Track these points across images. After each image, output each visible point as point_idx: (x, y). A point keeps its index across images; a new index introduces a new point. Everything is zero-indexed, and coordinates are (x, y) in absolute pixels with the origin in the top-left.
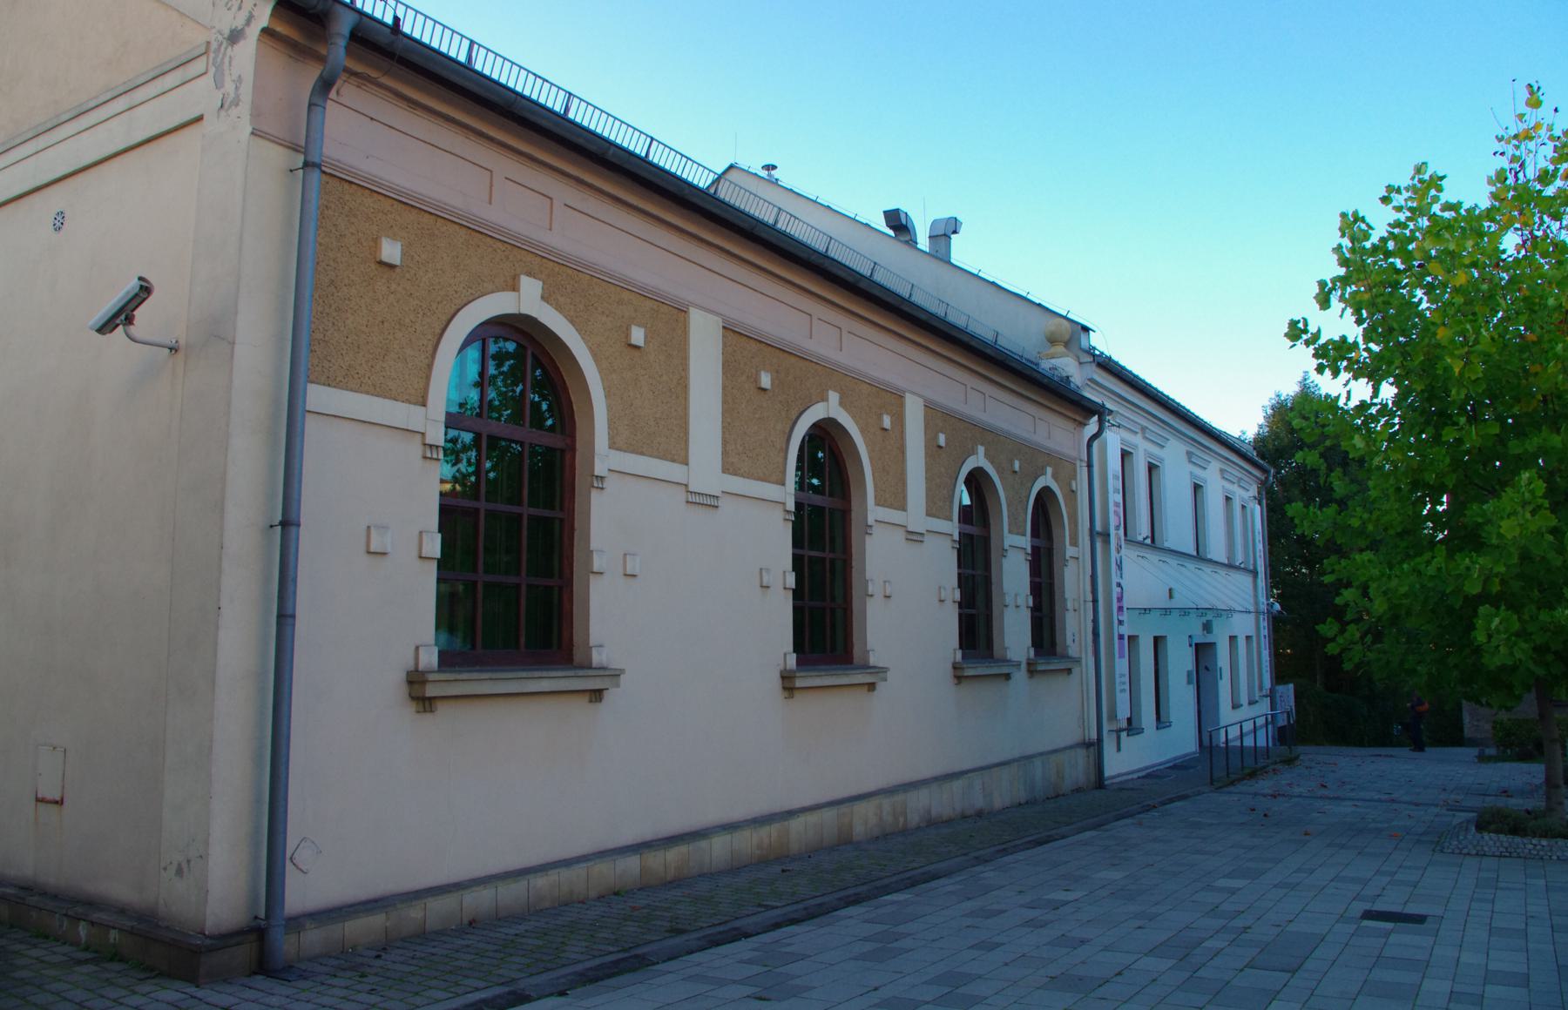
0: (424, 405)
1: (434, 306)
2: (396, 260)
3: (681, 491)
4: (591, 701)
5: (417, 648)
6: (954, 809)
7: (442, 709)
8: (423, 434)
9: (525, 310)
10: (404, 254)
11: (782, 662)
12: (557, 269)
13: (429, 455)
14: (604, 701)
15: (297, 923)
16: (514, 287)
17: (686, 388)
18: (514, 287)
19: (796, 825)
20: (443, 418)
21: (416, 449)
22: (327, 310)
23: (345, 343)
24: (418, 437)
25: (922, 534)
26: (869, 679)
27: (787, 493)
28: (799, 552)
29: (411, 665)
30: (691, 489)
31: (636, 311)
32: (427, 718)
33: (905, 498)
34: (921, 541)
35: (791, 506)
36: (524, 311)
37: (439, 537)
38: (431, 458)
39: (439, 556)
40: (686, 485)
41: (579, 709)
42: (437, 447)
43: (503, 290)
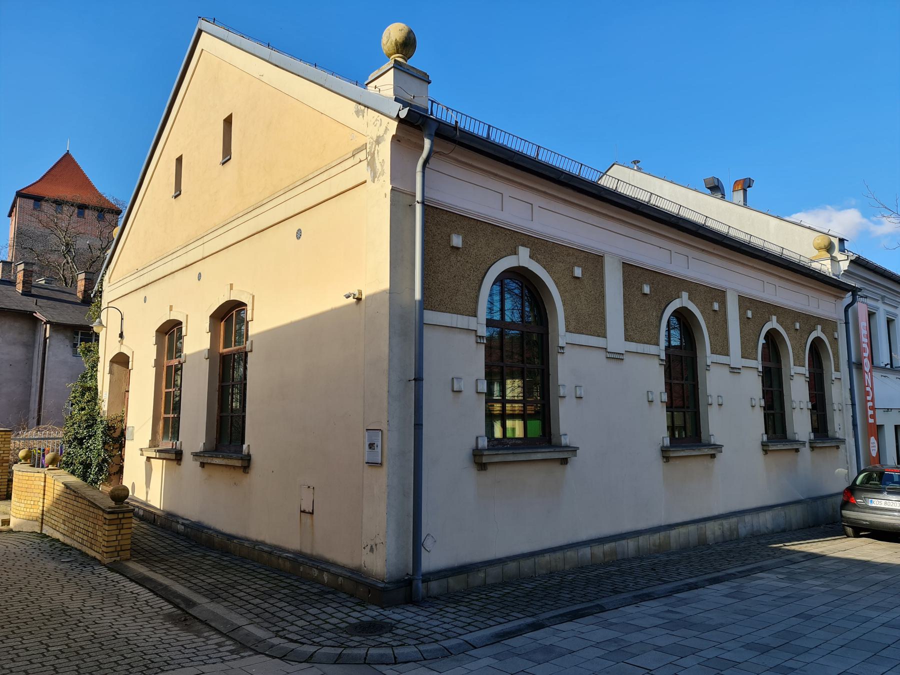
5: (477, 438)
8: (476, 331)
16: (515, 253)
21: (472, 338)
25: (739, 369)
33: (605, 330)
36: (521, 265)
42: (483, 337)
43: (511, 255)
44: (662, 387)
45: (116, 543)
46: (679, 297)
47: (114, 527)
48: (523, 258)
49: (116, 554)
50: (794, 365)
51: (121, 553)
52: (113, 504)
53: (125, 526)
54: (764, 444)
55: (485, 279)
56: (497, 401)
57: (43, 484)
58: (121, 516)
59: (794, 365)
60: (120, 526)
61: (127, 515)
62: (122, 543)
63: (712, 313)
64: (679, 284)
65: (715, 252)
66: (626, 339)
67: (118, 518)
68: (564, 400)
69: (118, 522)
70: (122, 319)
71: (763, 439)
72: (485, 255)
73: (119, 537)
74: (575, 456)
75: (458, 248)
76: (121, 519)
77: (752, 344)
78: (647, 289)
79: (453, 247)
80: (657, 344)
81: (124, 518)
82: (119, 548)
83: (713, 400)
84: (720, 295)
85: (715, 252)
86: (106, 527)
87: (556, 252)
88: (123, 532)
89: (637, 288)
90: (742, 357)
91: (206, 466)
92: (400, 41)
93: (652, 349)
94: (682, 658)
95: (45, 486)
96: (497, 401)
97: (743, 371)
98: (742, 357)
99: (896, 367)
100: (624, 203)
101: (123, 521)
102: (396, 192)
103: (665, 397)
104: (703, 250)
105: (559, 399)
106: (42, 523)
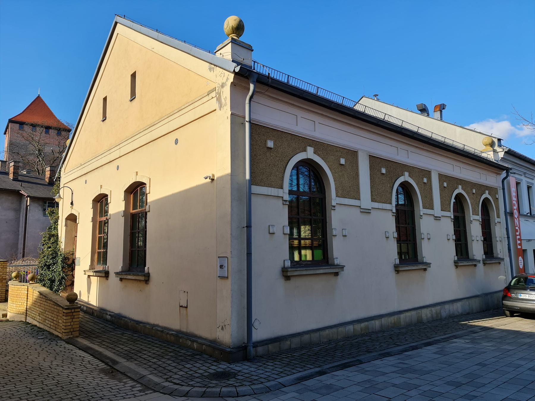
11: (394, 262)
13: (285, 203)
21: (281, 202)
24: (281, 198)
42: (287, 201)
44: (394, 229)
45: (70, 327)
47: (69, 317)
49: (70, 333)
50: (473, 215)
52: (68, 304)
53: (76, 317)
54: (455, 262)
56: (296, 239)
57: (26, 292)
58: (73, 311)
60: (72, 317)
61: (76, 310)
62: (74, 327)
63: (423, 184)
64: (403, 168)
66: (372, 201)
67: (71, 312)
69: (71, 314)
70: (72, 194)
71: (483, 258)
72: (287, 152)
73: (72, 324)
75: (271, 148)
79: (268, 148)
82: (72, 330)
83: (425, 236)
84: (353, 155)
86: (65, 318)
88: (74, 320)
90: (441, 210)
91: (123, 280)
95: (28, 294)
96: (296, 239)
97: (442, 219)
98: (441, 210)
101: (74, 314)
106: (26, 316)
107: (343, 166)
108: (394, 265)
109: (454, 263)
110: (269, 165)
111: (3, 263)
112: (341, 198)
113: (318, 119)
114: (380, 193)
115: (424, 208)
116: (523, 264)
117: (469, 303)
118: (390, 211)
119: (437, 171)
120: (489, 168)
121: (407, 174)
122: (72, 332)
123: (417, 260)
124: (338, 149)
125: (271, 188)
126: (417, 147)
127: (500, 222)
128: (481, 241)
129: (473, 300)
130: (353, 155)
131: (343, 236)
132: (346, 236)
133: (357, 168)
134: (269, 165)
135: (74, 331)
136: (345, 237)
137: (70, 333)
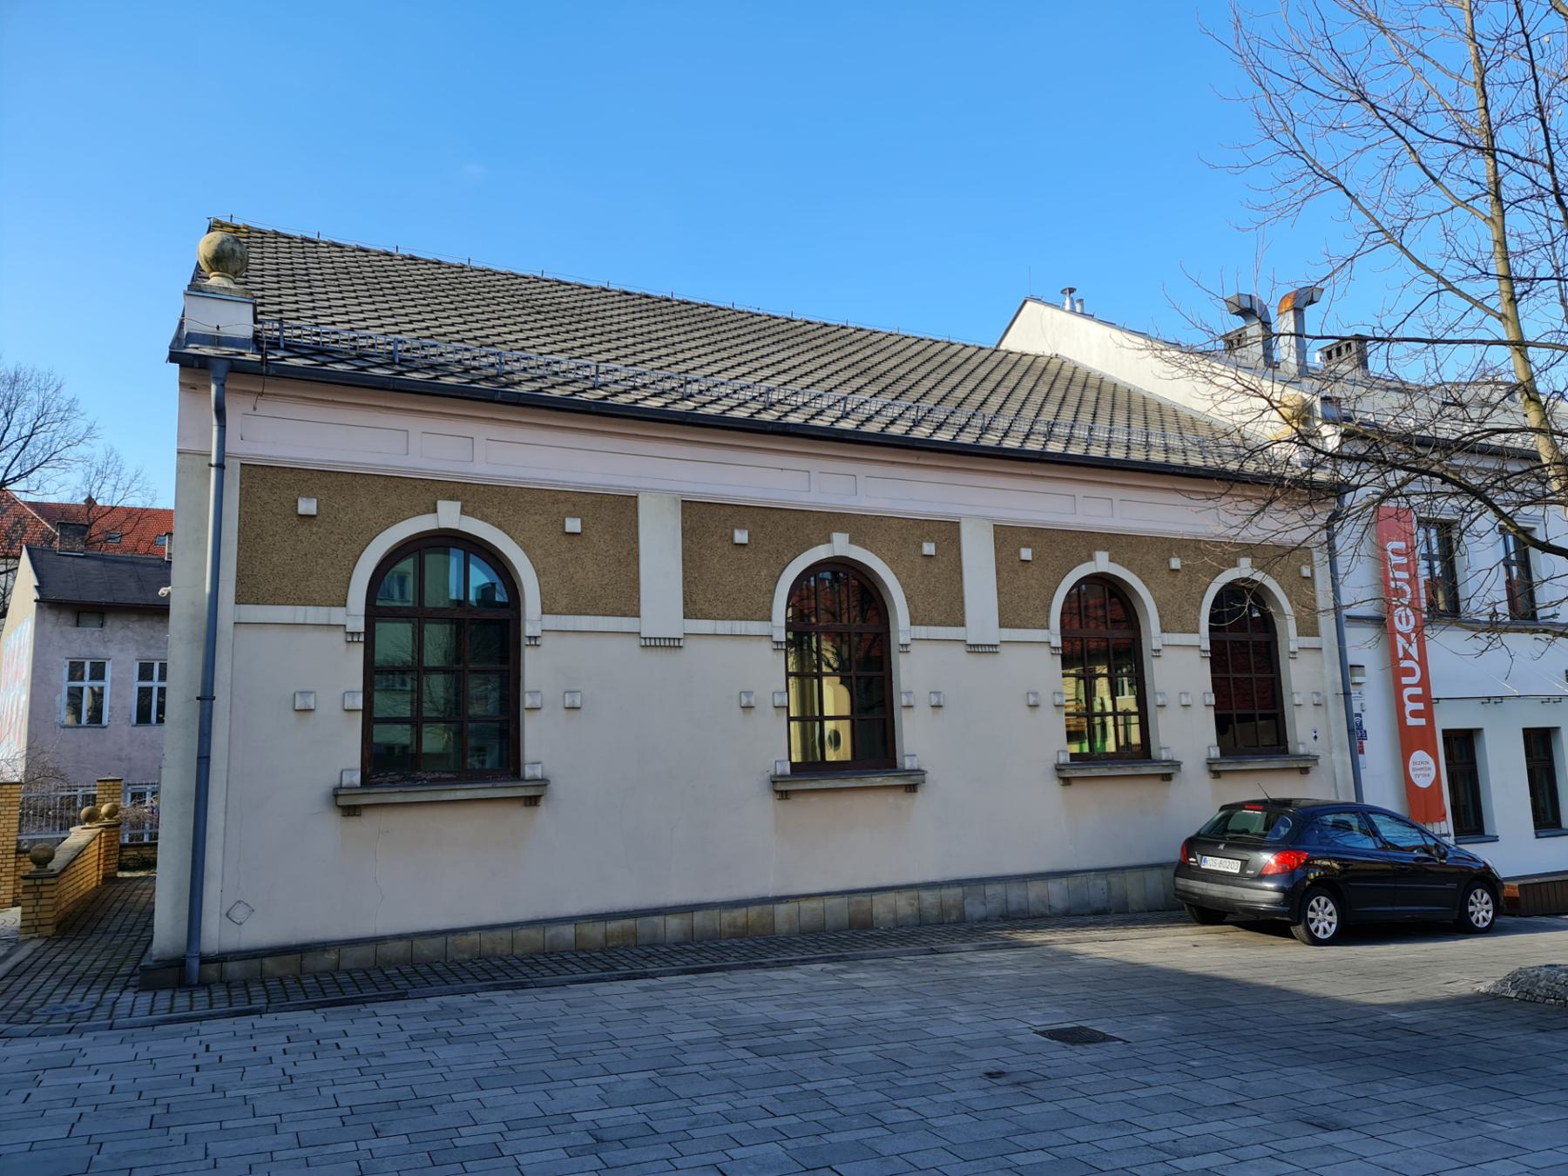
0: (770, 620)
1: (355, 537)
2: (1030, 558)
3: (634, 643)
4: (526, 805)
6: (1006, 901)
7: (1223, 776)
9: (838, 553)
10: (937, 549)
11: (1206, 752)
12: (482, 489)
14: (344, 819)
15: (205, 960)
16: (829, 541)
17: (637, 556)
18: (829, 541)
19: (782, 910)
20: (784, 624)
21: (340, 637)
22: (255, 554)
23: (271, 574)
25: (996, 646)
26: (531, 792)
27: (1203, 638)
28: (1215, 675)
29: (337, 783)
30: (969, 642)
31: (574, 505)
32: (353, 822)
33: (963, 615)
34: (997, 652)
35: (1206, 645)
36: (442, 526)
37: (1213, 695)
38: (646, 646)
39: (1214, 703)
40: (639, 633)
41: (518, 814)
44: (1208, 685)
45: (33, 916)
46: (1090, 558)
47: (31, 896)
48: (1102, 563)
49: (33, 929)
50: (1163, 631)
51: (40, 929)
52: (34, 868)
53: (45, 895)
54: (1210, 763)
55: (364, 553)
56: (1109, 714)
58: (38, 882)
59: (1163, 631)
60: (37, 895)
61: (47, 881)
62: (40, 916)
63: (919, 560)
64: (1090, 541)
65: (921, 462)
66: (1001, 626)
67: (35, 885)
68: (1164, 710)
69: (35, 889)
71: (1058, 759)
72: (370, 519)
73: (37, 909)
74: (1179, 770)
75: (1177, 570)
76: (38, 886)
77: (1037, 602)
78: (741, 537)
79: (1305, 578)
80: (1196, 631)
81: (42, 885)
82: (36, 923)
83: (922, 700)
84: (948, 532)
85: (921, 462)
87: (525, 501)
88: (42, 902)
89: (721, 537)
90: (1001, 626)
92: (209, 256)
93: (755, 627)
94: (808, 1170)
96: (1109, 714)
97: (1003, 650)
98: (1001, 626)
99: (1543, 618)
100: (820, 434)
101: (42, 889)
102: (183, 456)
103: (1212, 699)
104: (893, 463)
105: (1296, 708)
107: (576, 538)
108: (1056, 765)
109: (1056, 773)
110: (306, 555)
111: (8, 787)
112: (563, 617)
113: (1116, 494)
114: (726, 594)
115: (550, 613)
116: (1411, 766)
117: (1109, 884)
118: (962, 644)
119: (985, 518)
120: (918, 458)
121: (1245, 562)
122: (36, 926)
123: (1150, 758)
124: (562, 497)
125: (326, 609)
126: (893, 463)
127: (1320, 649)
128: (1207, 706)
129: (1157, 873)
130: (948, 532)
131: (1031, 706)
132: (911, 707)
133: (632, 539)
134: (306, 555)
135: (40, 925)
136: (305, 714)
137: (33, 929)
